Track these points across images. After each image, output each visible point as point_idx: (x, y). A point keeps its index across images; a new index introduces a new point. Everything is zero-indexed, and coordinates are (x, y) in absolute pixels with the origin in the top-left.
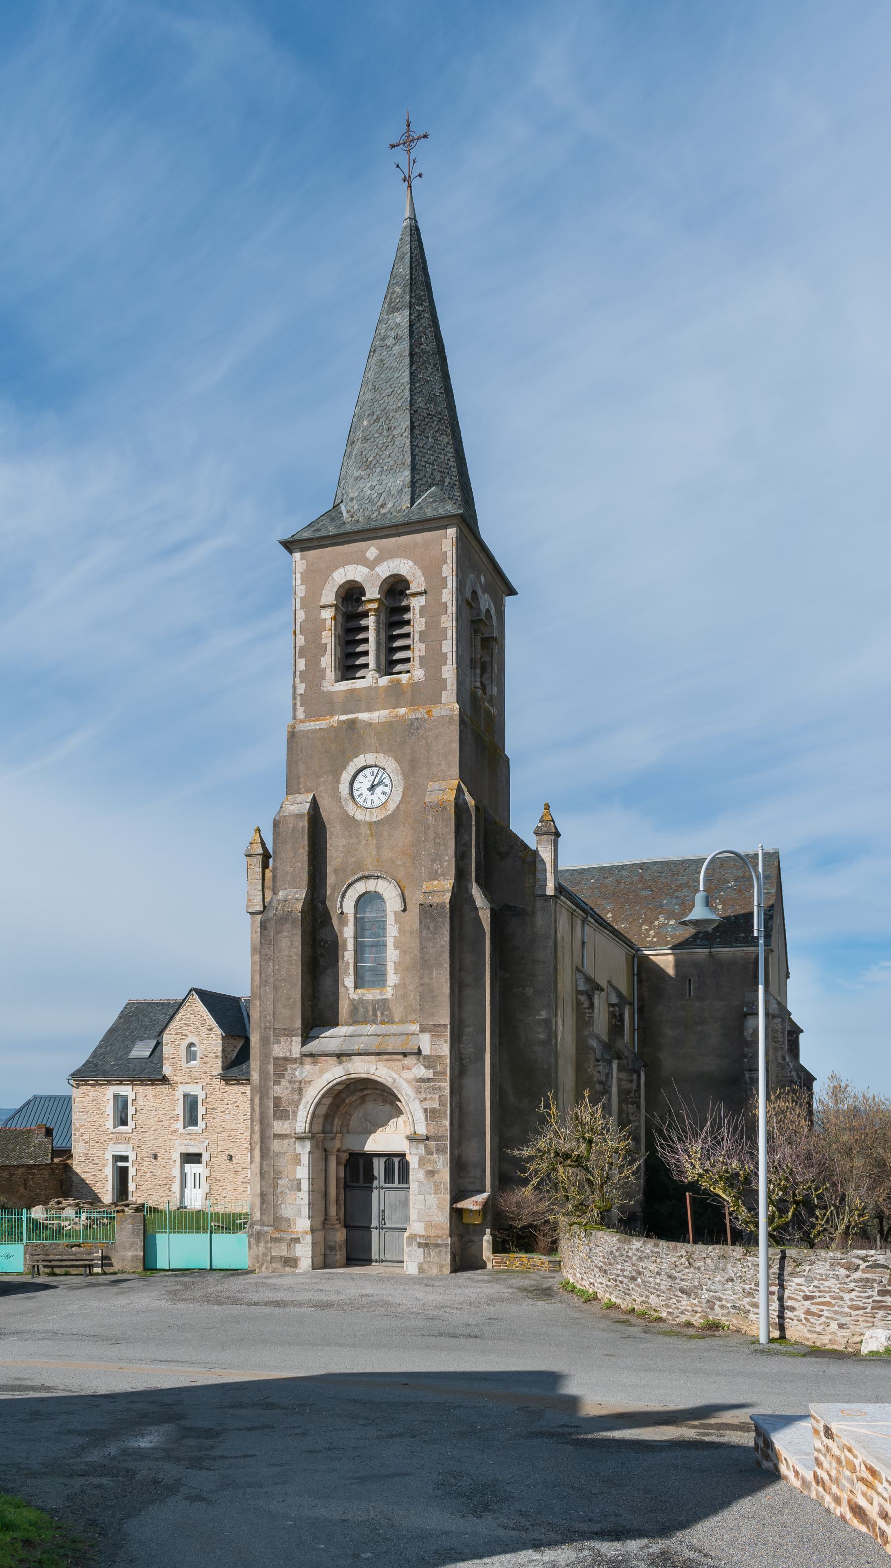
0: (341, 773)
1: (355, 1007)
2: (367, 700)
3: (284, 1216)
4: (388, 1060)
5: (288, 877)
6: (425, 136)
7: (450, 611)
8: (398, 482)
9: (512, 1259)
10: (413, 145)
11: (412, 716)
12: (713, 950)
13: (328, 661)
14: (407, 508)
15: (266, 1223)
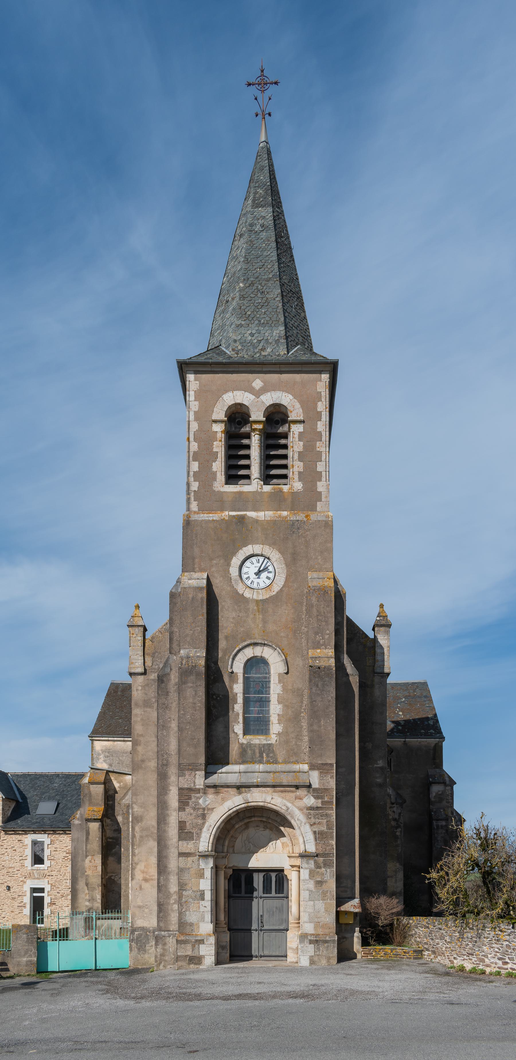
0: (232, 559)
1: (244, 749)
2: (254, 502)
3: (189, 921)
4: (282, 792)
5: (188, 639)
6: (276, 83)
7: (323, 439)
8: (274, 334)
9: (377, 950)
10: (266, 87)
11: (293, 518)
12: (407, 740)
13: (219, 466)
14: (285, 354)
15: (163, 929)
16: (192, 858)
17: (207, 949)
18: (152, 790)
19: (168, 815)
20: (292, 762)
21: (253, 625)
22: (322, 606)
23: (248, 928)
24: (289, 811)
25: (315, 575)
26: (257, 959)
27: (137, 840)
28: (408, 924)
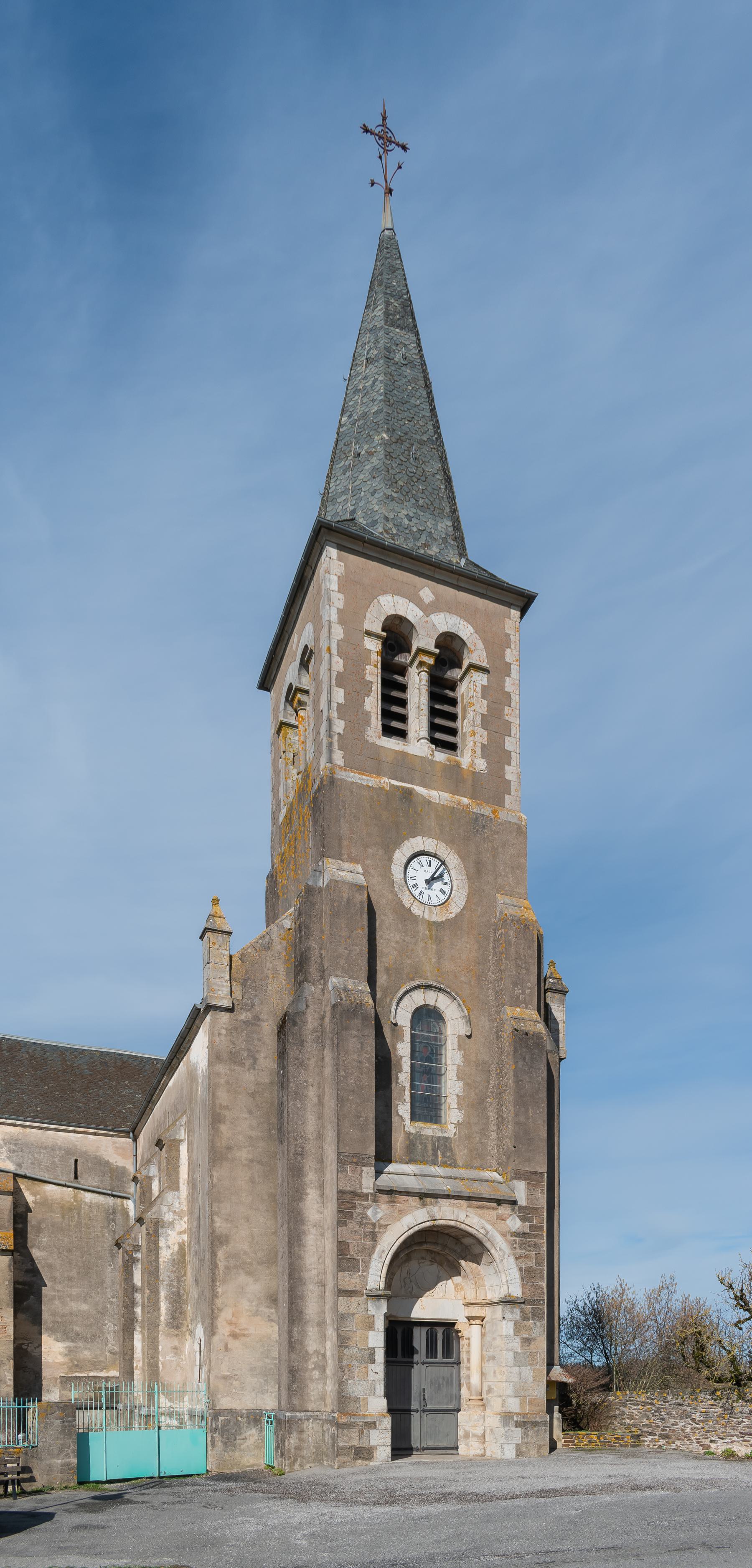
0: (394, 851)
1: (412, 1142)
4: (479, 1207)
5: (342, 962)
6: (404, 148)
9: (580, 1437)
11: (477, 810)
15: (298, 1408)
16: (357, 1299)
17: (381, 1436)
18: (244, 1195)
19: (304, 1232)
20: (476, 1168)
21: (423, 958)
22: (522, 946)
23: (406, 1407)
24: (489, 1236)
25: (507, 900)
26: (419, 1453)
27: (221, 1272)
28: (603, 1402)
